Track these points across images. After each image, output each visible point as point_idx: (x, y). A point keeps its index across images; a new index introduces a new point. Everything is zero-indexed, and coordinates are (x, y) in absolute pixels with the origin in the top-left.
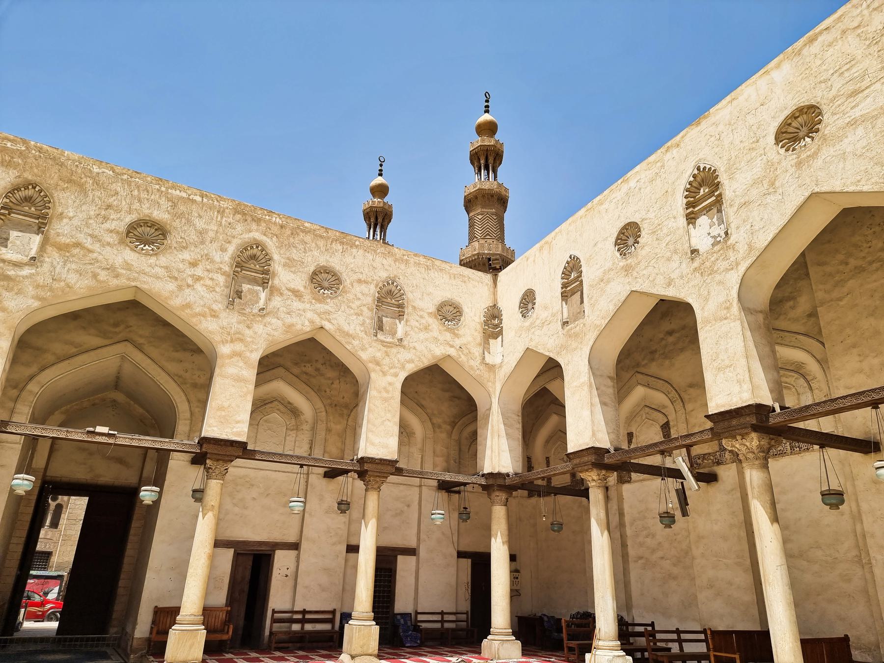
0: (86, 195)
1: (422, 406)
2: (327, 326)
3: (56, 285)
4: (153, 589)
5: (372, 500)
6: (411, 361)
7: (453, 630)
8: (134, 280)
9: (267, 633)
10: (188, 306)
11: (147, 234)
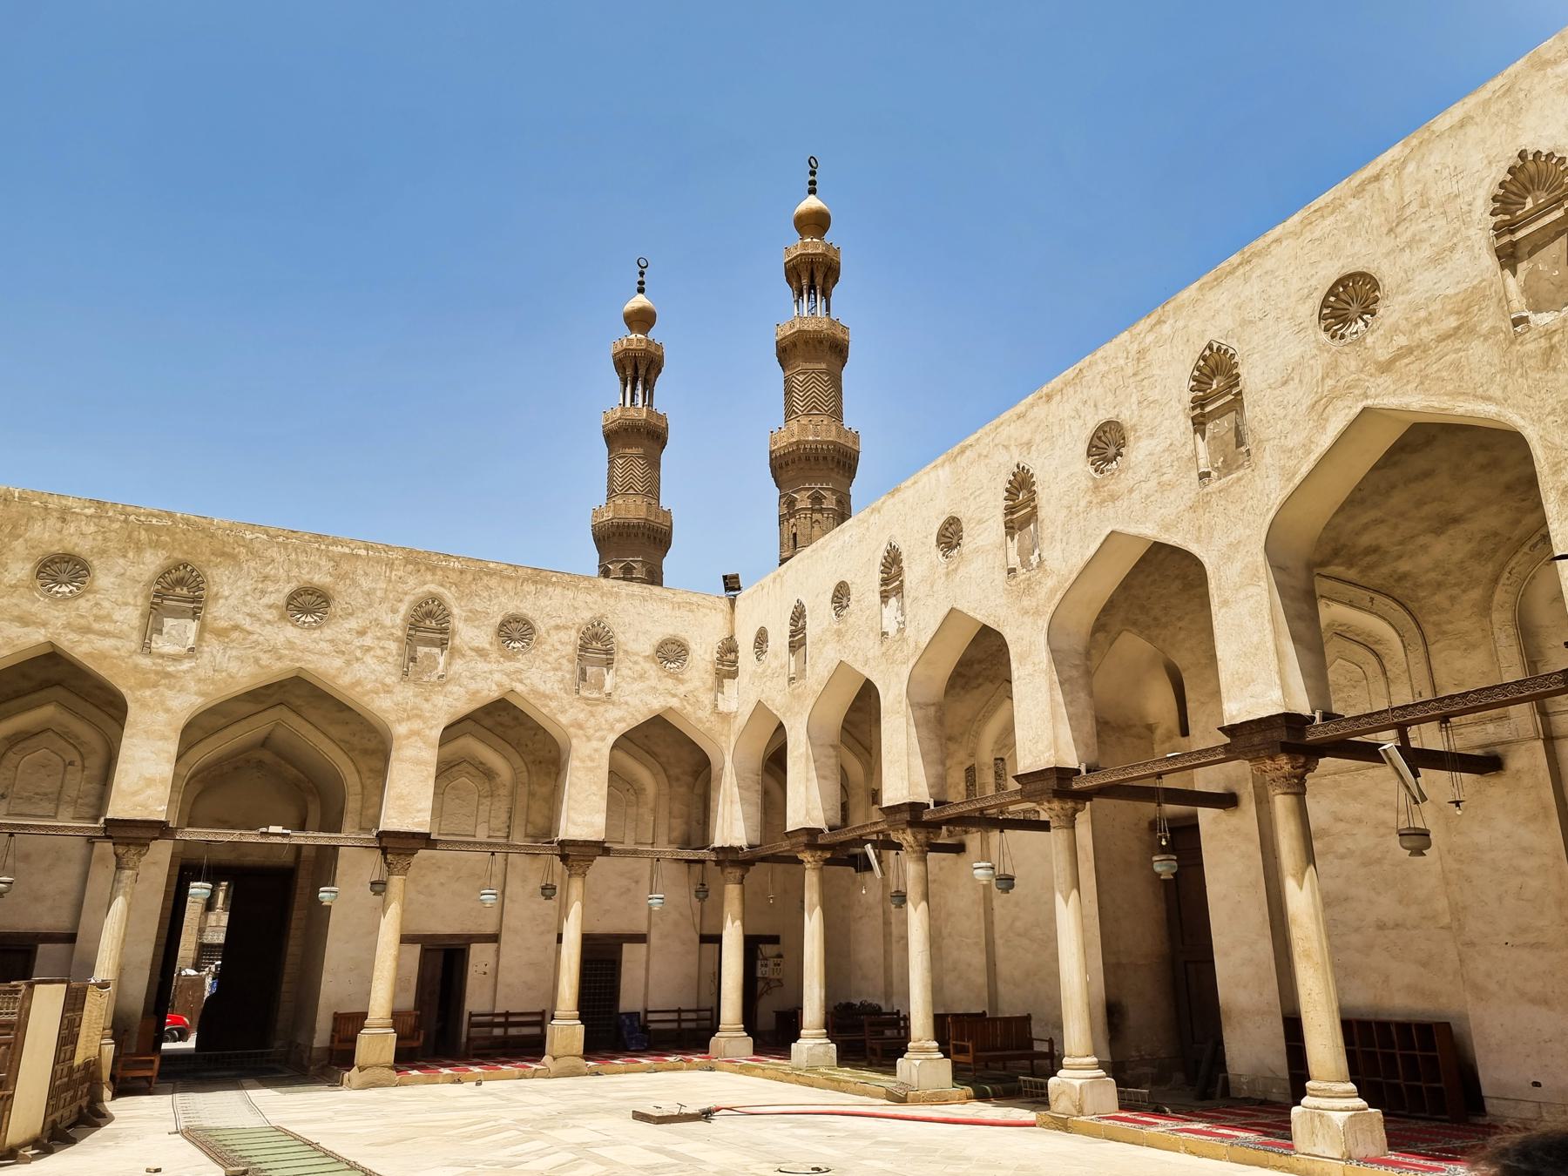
0: (241, 569)
1: (653, 755)
2: (519, 687)
3: (218, 676)
4: (332, 992)
5: (576, 886)
7: (690, 1030)
8: (298, 660)
9: (464, 1039)
10: (358, 683)
11: (309, 603)
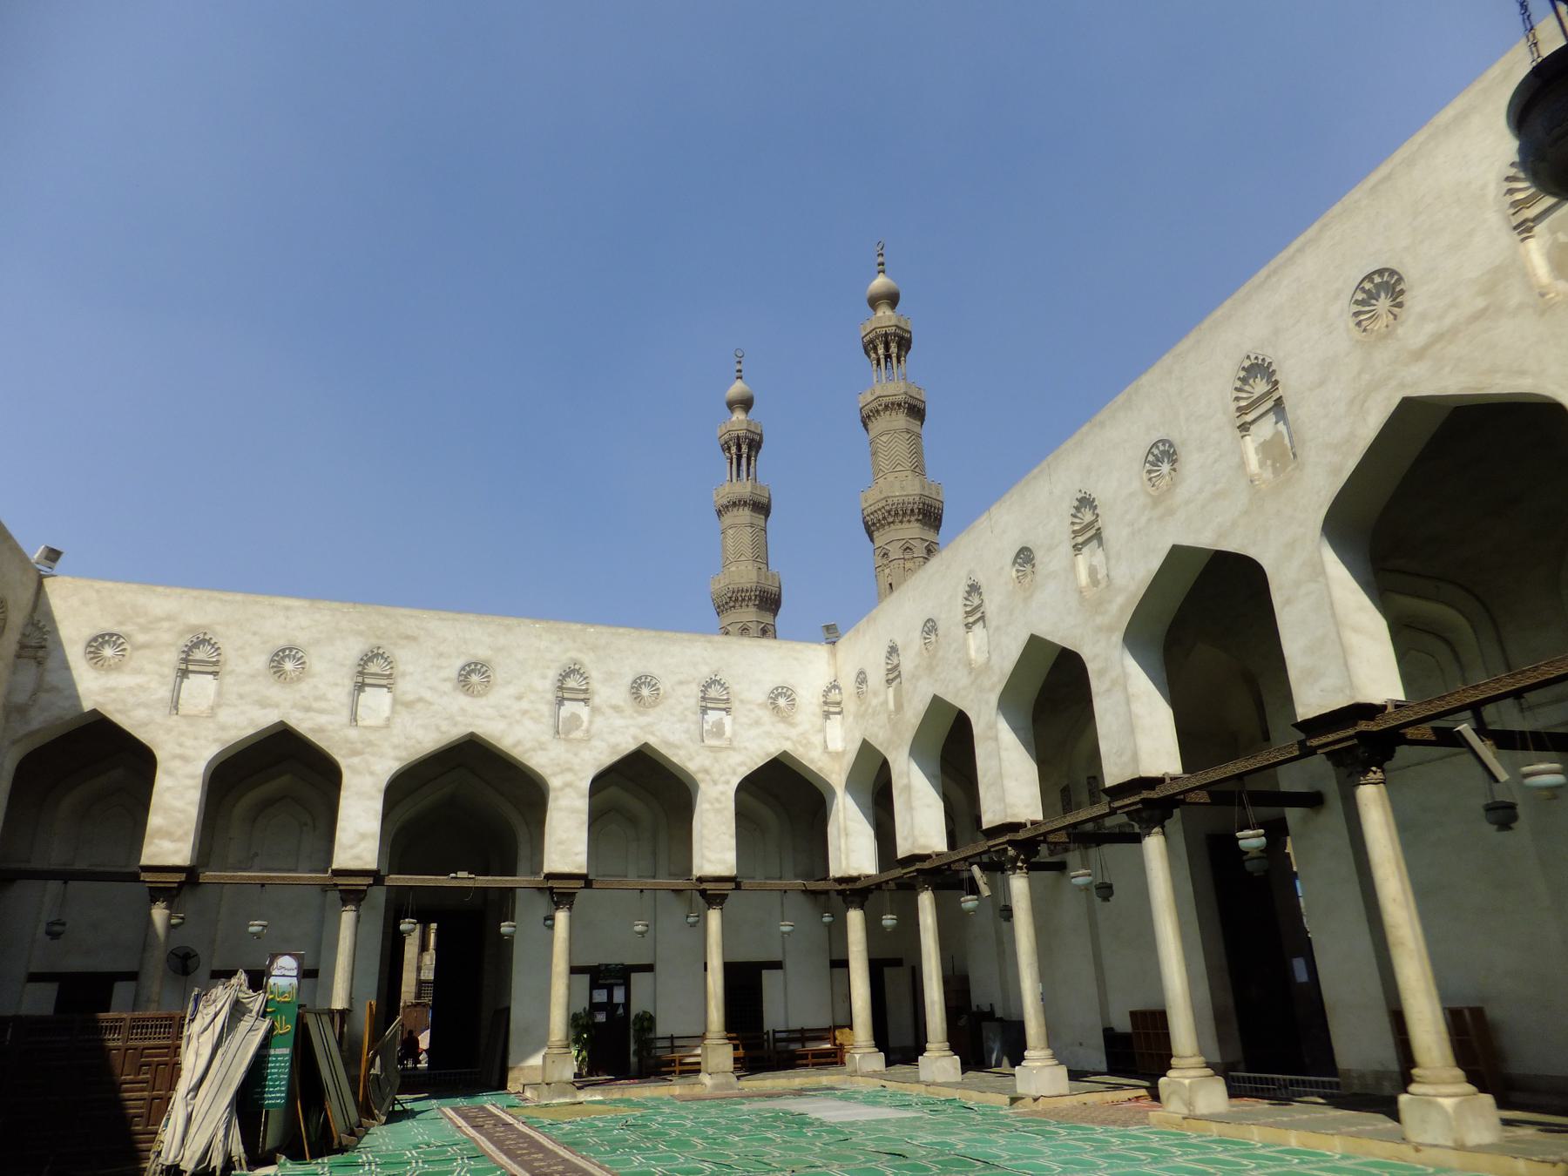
6: (742, 764)
